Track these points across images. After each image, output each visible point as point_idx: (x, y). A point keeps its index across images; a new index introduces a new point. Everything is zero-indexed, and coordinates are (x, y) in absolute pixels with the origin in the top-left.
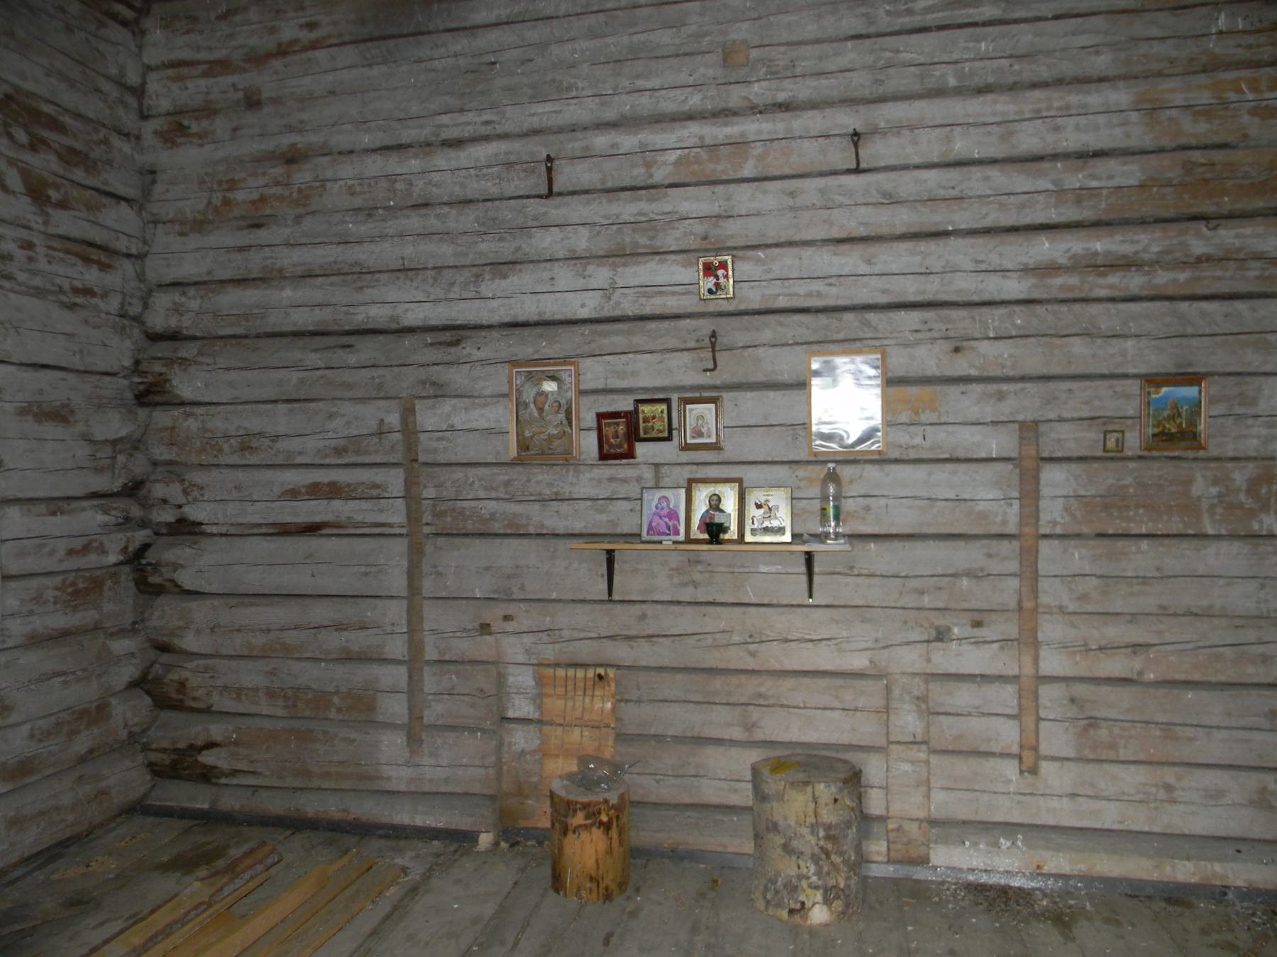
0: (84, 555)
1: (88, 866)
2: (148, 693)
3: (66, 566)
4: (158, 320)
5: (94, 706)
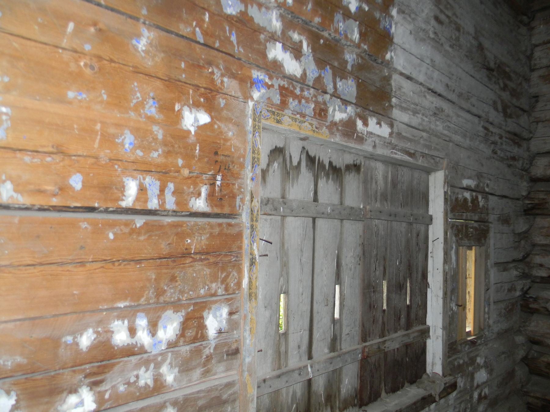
2: (527, 365)
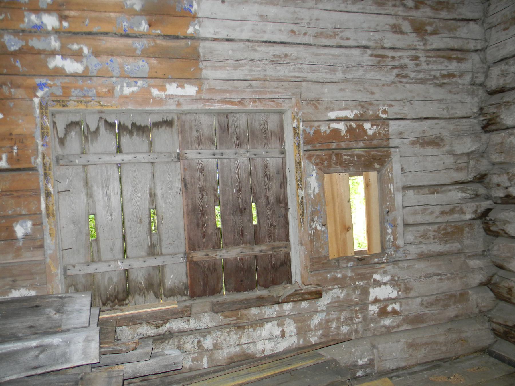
0: (451, 214)
1: (449, 378)
2: (492, 290)
3: (440, 220)
4: (493, 84)
5: (458, 293)
